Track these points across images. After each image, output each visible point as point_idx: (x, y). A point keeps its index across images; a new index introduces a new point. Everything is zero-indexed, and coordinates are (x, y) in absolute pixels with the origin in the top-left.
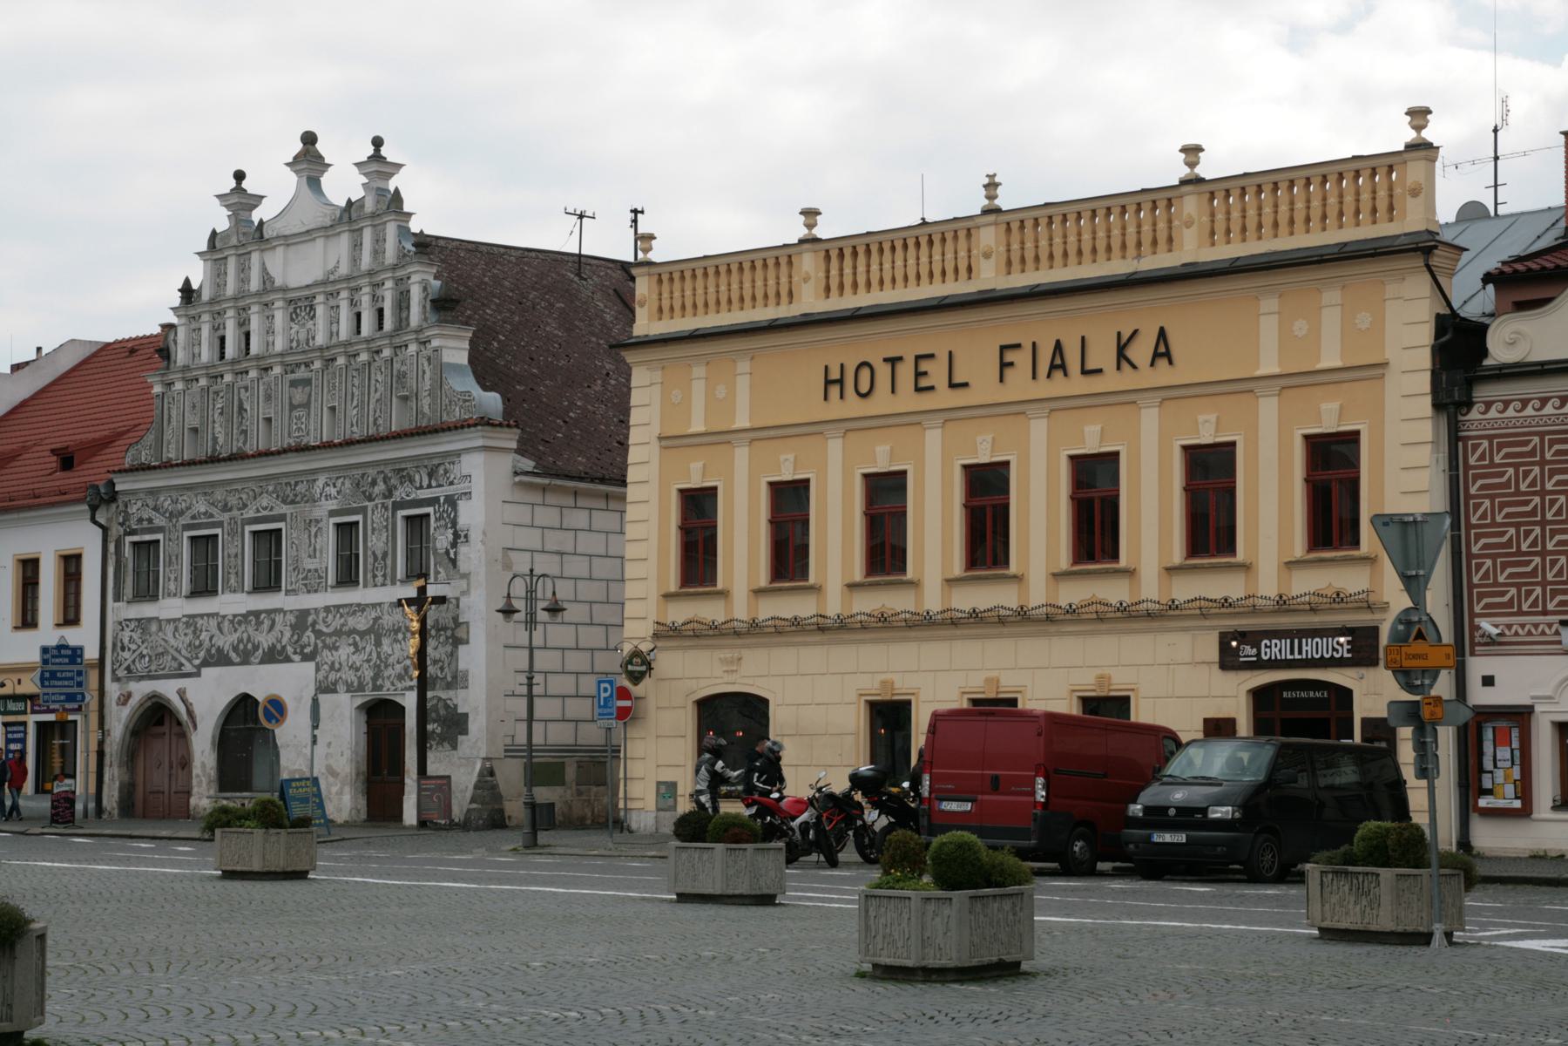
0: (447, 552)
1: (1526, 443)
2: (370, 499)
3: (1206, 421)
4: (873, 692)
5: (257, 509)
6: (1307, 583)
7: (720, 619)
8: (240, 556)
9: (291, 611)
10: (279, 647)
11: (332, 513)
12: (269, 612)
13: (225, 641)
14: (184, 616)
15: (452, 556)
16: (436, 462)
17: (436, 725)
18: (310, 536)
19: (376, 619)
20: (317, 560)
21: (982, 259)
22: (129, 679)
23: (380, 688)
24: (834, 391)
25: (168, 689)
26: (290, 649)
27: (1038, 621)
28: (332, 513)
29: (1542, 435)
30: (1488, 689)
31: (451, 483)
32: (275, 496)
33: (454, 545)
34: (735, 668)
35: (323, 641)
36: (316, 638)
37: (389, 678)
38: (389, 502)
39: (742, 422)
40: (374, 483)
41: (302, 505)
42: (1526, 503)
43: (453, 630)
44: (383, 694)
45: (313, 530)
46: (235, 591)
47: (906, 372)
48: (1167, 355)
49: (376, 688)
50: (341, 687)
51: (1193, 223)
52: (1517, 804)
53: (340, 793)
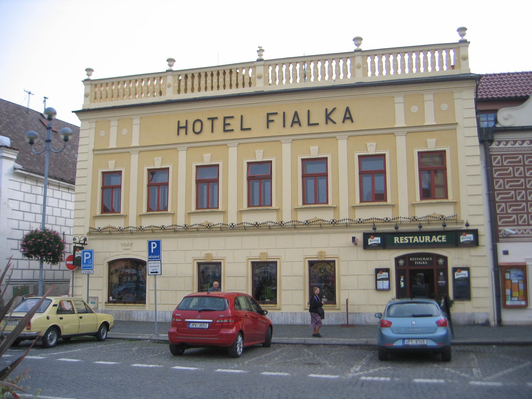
1: (516, 158)
3: (371, 145)
4: (201, 258)
6: (422, 213)
7: (123, 226)
21: (257, 79)
24: (182, 131)
27: (289, 228)
29: (523, 155)
30: (506, 256)
34: (129, 248)
39: (135, 143)
42: (518, 181)
47: (219, 124)
48: (351, 118)
51: (361, 67)
52: (523, 303)
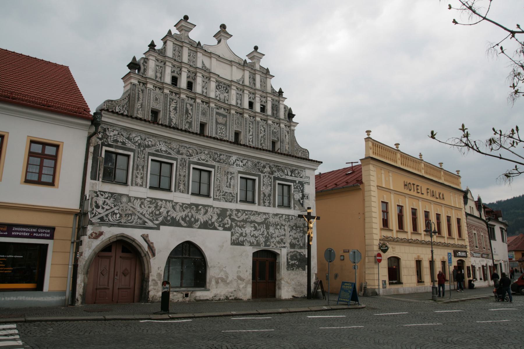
0: (299, 201)
2: (262, 172)
5: (199, 159)
8: (187, 177)
9: (217, 208)
10: (210, 222)
11: (240, 172)
12: (204, 206)
13: (178, 215)
14: (148, 198)
15: (301, 202)
16: (294, 168)
17: (296, 261)
18: (227, 178)
19: (266, 219)
20: (231, 189)
22: (100, 225)
23: (269, 246)
25: (136, 234)
26: (216, 225)
28: (240, 172)
31: (301, 177)
32: (209, 156)
33: (302, 198)
35: (236, 224)
36: (232, 222)
37: (273, 242)
38: (272, 176)
40: (264, 167)
41: (224, 164)
43: (303, 228)
44: (270, 248)
45: (230, 177)
46: (183, 192)
49: (266, 245)
50: (246, 243)
53: (245, 287)
